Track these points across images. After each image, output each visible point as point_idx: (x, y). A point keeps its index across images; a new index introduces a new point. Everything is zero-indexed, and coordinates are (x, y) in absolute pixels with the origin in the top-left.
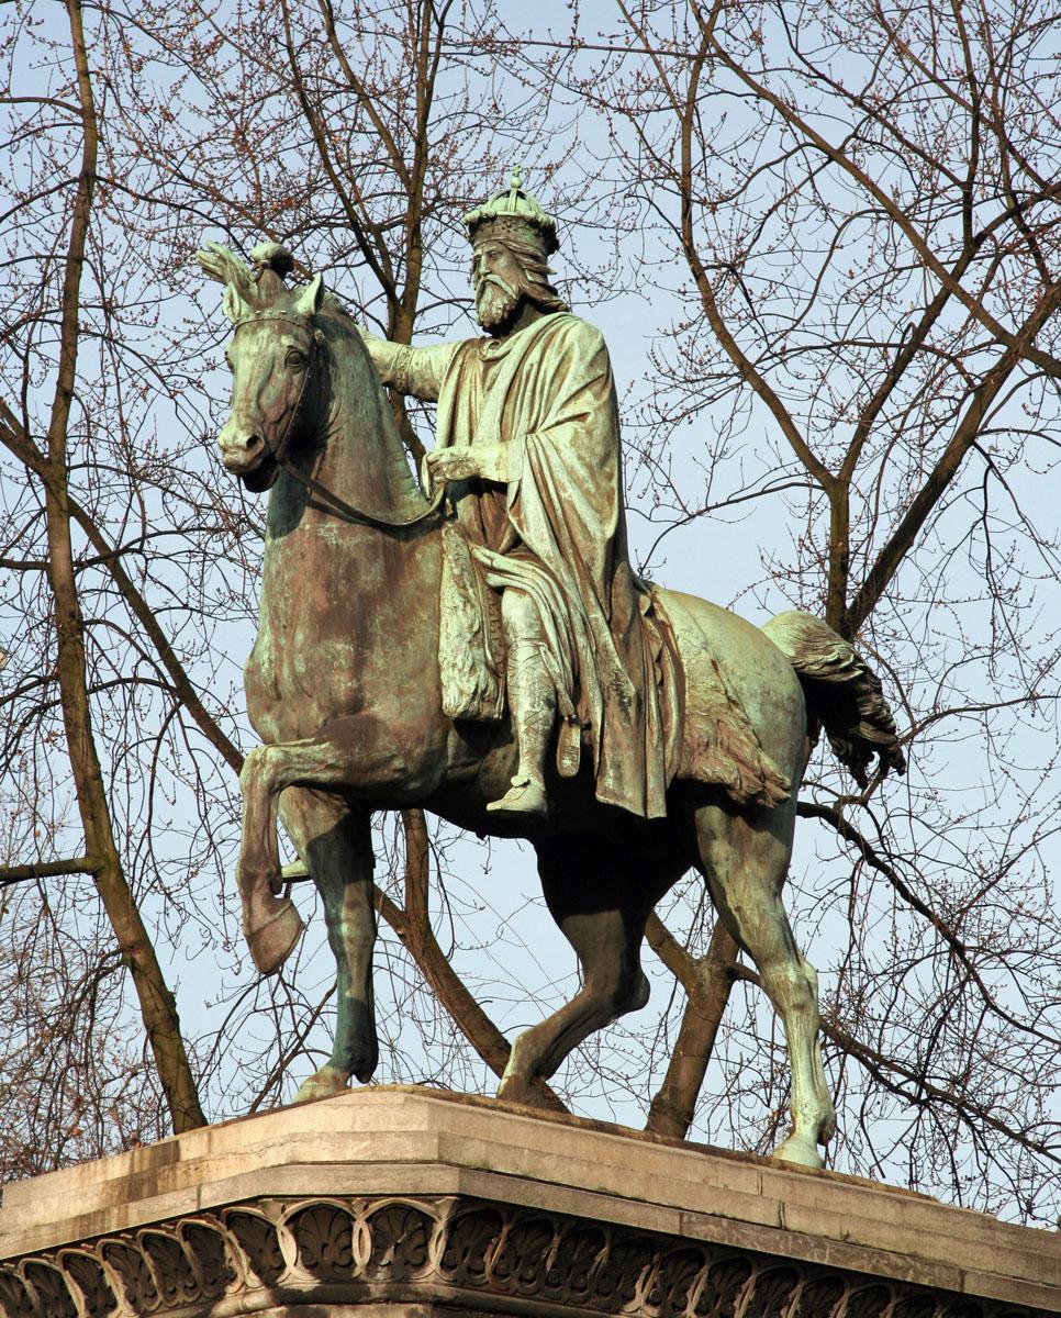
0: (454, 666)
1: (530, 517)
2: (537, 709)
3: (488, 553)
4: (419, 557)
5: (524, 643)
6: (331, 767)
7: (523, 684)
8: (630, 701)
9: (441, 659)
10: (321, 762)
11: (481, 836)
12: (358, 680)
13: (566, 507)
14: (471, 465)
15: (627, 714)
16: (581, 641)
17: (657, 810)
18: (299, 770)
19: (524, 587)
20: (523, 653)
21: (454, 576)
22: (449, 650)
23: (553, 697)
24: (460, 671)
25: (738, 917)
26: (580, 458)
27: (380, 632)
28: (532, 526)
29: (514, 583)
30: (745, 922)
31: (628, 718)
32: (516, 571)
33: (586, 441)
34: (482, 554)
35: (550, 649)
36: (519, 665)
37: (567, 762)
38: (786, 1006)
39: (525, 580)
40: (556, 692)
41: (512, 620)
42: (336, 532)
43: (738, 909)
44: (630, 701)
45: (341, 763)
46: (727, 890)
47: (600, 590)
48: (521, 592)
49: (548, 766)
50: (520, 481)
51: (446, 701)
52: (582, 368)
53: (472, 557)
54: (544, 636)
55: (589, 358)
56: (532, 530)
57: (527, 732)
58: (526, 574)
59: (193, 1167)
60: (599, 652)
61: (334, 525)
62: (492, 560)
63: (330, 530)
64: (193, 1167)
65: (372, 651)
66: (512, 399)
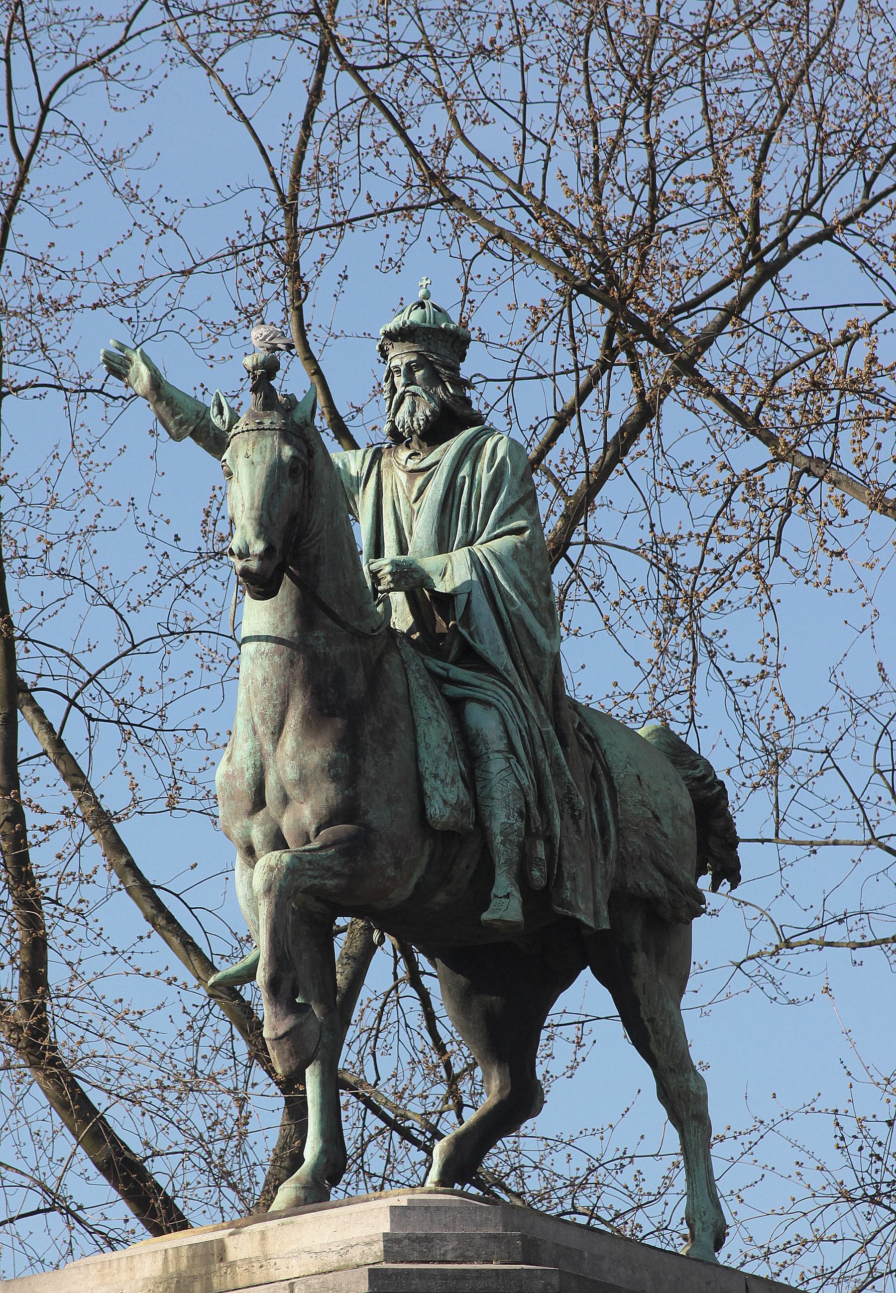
0: (436, 776)
1: (484, 630)
2: (512, 821)
3: (440, 663)
4: (387, 666)
5: (497, 755)
6: (336, 875)
7: (498, 795)
8: (580, 814)
9: (422, 769)
10: (328, 869)
11: (635, 975)
12: (354, 789)
13: (515, 620)
14: (415, 575)
15: (578, 827)
16: (541, 754)
17: (606, 926)
18: (310, 876)
19: (490, 699)
20: (497, 765)
21: (422, 687)
22: (430, 761)
23: (524, 810)
24: (442, 781)
25: (650, 1028)
26: (522, 572)
27: (369, 741)
28: (487, 639)
29: (478, 695)
30: (656, 1033)
31: (579, 831)
32: (478, 682)
33: (526, 555)
34: (436, 665)
35: (519, 761)
36: (492, 776)
37: (536, 873)
38: (684, 1115)
39: (489, 693)
40: (527, 804)
41: (485, 731)
42: (323, 640)
43: (651, 1020)
44: (580, 814)
45: (346, 870)
46: (641, 1002)
47: (550, 705)
48: (487, 704)
49: (522, 879)
50: (470, 594)
51: (430, 811)
52: (515, 486)
53: (429, 670)
54: (511, 748)
55: (520, 473)
56: (487, 642)
57: (503, 843)
58: (491, 688)
59: (257, 1265)
60: (555, 763)
61: (321, 634)
62: (447, 670)
63: (318, 638)
64: (257, 1265)
65: (365, 760)
66: (448, 512)
